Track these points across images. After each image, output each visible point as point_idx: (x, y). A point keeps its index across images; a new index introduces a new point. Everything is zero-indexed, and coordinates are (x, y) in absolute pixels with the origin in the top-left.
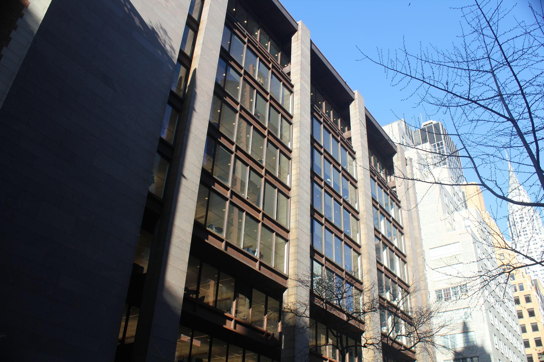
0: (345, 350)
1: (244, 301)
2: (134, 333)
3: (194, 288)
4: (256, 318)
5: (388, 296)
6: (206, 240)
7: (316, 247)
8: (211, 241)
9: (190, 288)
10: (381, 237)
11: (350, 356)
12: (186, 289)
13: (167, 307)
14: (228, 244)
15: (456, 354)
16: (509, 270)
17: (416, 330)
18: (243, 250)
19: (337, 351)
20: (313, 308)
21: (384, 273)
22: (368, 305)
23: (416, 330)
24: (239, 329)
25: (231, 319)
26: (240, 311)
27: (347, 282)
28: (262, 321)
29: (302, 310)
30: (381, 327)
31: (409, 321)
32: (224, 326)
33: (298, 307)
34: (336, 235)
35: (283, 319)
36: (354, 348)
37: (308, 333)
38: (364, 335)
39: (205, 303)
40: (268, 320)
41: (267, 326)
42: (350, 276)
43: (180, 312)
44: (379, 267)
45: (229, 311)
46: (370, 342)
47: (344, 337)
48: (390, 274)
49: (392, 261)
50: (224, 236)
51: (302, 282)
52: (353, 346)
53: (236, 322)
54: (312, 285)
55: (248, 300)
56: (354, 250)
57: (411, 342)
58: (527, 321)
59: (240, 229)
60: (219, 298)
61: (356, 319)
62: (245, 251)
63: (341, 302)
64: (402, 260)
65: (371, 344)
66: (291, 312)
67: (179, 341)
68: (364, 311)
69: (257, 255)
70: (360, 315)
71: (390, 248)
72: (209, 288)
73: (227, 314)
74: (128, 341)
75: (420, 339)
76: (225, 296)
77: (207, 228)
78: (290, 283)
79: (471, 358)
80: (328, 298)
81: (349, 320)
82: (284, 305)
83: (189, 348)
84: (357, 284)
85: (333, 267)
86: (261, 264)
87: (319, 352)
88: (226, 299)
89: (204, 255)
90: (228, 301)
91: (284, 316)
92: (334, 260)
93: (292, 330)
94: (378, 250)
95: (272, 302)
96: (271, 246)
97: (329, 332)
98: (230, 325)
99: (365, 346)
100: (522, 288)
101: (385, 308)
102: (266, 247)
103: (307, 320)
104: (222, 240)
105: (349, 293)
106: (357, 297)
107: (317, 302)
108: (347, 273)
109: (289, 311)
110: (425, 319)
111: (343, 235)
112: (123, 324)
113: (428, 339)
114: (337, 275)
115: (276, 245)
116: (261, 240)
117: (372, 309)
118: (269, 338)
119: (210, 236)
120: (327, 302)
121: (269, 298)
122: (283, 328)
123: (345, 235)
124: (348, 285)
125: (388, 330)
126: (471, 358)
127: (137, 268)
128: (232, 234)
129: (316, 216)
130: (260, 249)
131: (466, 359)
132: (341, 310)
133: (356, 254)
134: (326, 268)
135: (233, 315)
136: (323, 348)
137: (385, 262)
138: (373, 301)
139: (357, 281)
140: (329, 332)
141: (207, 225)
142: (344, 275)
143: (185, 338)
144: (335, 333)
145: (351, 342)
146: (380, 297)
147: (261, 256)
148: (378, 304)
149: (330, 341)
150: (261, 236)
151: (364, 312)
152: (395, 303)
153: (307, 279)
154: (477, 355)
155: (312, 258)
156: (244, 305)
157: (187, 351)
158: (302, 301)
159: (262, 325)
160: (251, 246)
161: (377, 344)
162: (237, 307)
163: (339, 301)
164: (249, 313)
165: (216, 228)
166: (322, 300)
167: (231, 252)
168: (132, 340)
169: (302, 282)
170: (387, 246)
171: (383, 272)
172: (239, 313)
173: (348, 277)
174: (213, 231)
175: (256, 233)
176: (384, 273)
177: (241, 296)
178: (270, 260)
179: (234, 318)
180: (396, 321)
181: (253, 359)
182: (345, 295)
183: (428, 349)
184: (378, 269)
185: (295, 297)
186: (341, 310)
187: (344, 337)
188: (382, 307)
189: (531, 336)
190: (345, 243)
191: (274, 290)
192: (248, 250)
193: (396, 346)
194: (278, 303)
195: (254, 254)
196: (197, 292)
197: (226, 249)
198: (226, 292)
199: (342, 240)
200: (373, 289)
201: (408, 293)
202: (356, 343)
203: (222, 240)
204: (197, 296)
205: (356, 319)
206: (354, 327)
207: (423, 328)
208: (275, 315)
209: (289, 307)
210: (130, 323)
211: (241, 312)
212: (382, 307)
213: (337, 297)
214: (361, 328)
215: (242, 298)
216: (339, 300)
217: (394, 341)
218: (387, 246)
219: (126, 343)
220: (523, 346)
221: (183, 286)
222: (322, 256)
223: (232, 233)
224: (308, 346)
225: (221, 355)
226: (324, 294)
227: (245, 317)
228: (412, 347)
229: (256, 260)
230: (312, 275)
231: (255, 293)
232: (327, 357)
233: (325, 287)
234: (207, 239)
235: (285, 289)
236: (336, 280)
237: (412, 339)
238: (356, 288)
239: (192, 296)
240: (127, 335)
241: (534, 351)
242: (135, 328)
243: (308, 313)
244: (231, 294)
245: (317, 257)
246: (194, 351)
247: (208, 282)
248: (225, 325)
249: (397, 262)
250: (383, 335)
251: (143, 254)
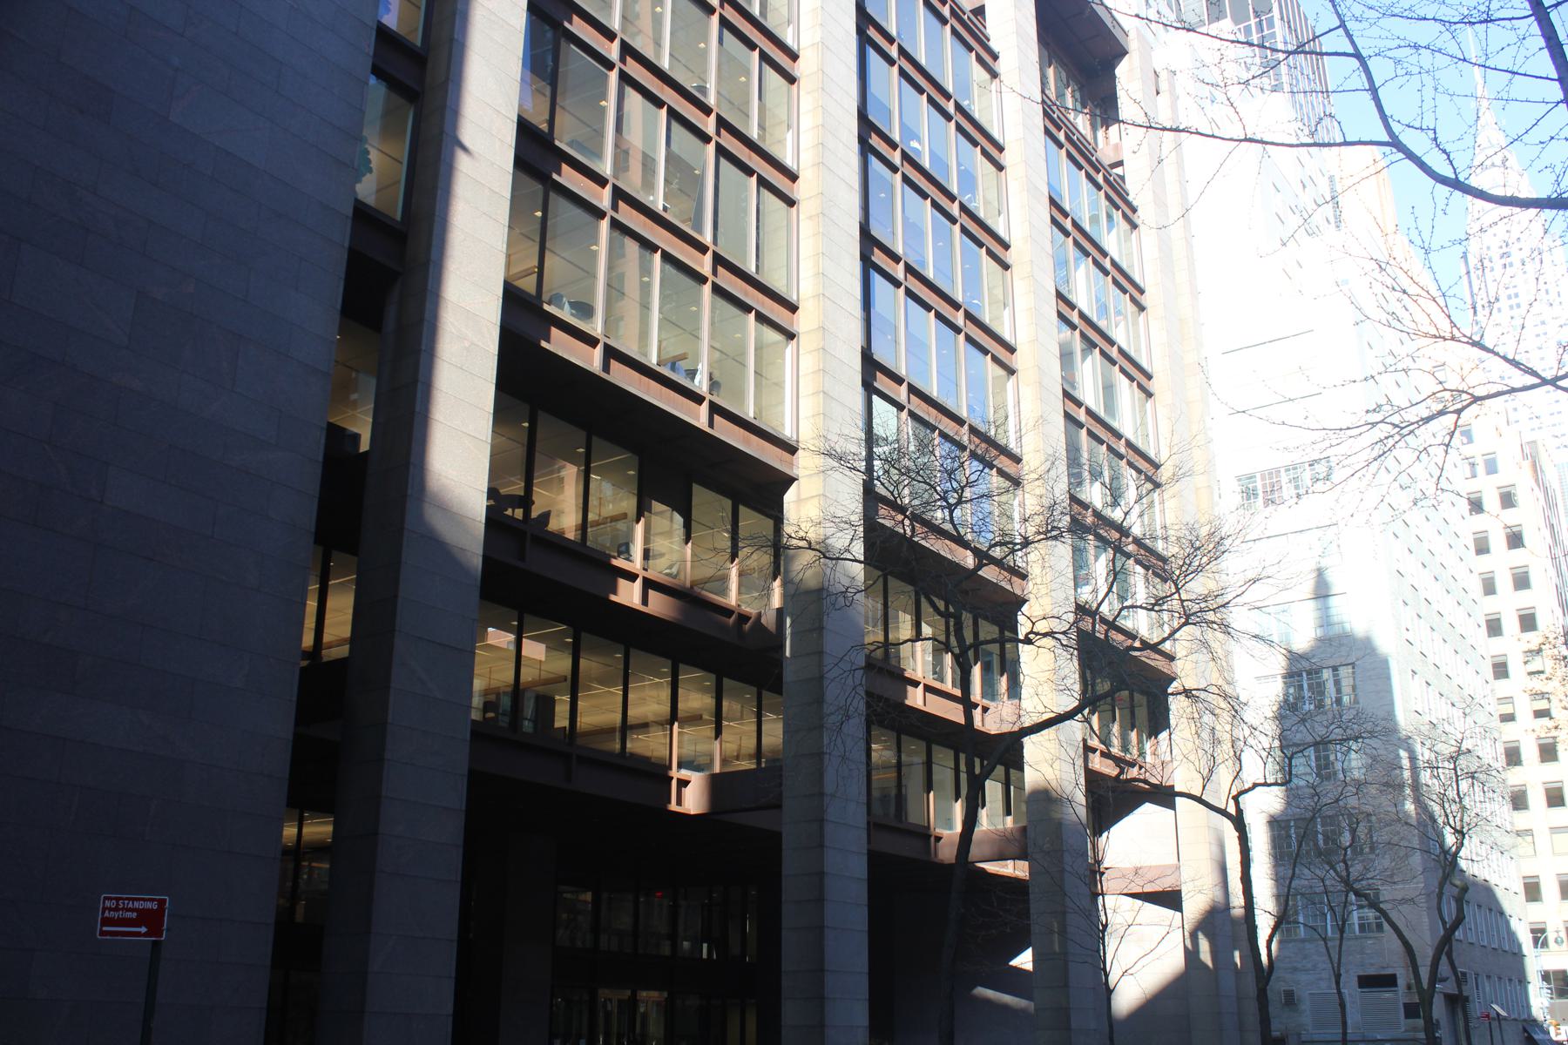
8: (559, 344)
25: (632, 577)
73: (619, 563)
135: (636, 564)
167: (622, 377)
197: (606, 368)
218: (1095, 346)
235: (789, 481)
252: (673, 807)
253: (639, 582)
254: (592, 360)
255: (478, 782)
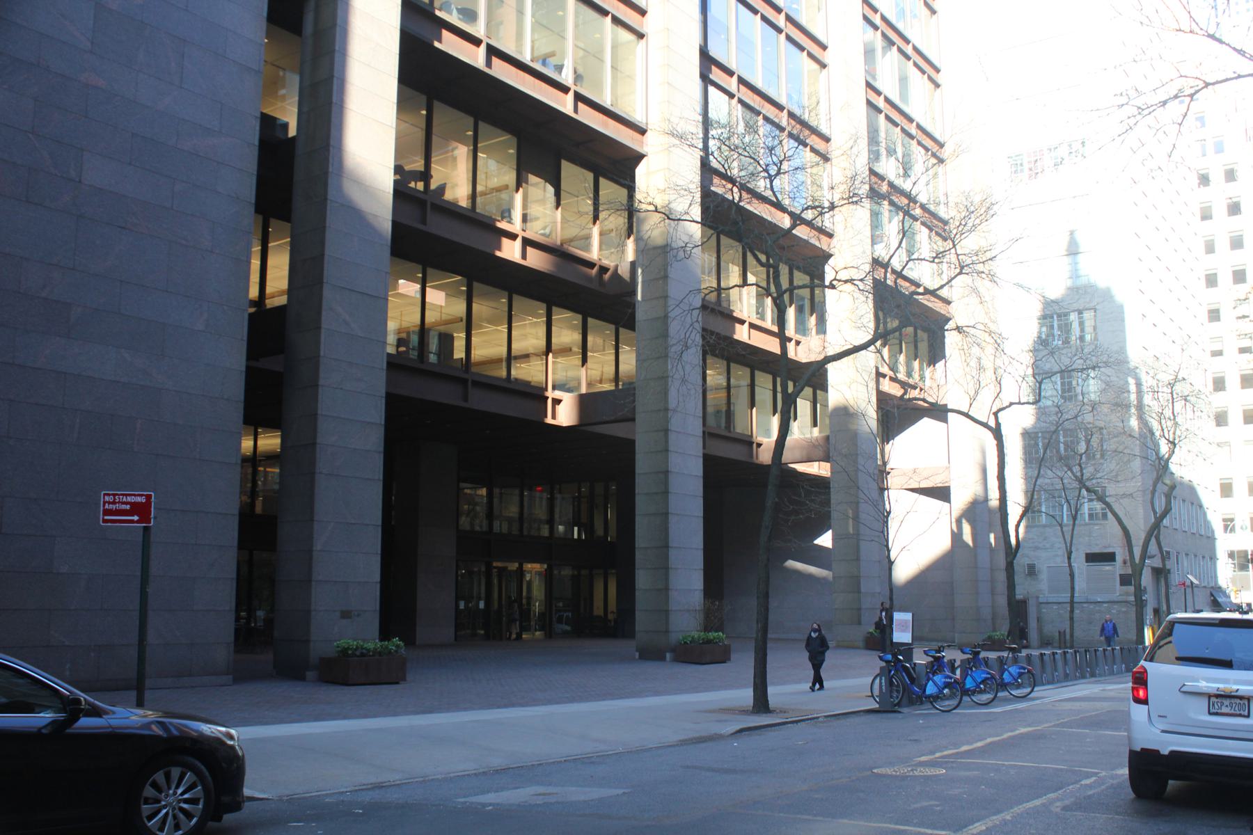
0: (786, 297)
1: (539, 189)
2: (284, 285)
3: (418, 165)
4: (572, 232)
5: (889, 168)
6: (436, 44)
7: (714, 52)
8: (449, 44)
9: (407, 168)
10: (877, 20)
11: (800, 310)
12: (398, 169)
13: (356, 215)
14: (492, 51)
15: (1048, 304)
16: (1192, 91)
17: (954, 246)
18: (531, 64)
19: (769, 301)
20: (708, 196)
21: (884, 109)
22: (843, 187)
23: (954, 246)
24: (535, 260)
25: (513, 237)
26: (534, 218)
27: (791, 135)
28: (588, 238)
29: (680, 206)
30: (872, 245)
31: (937, 225)
32: (498, 254)
33: (672, 197)
34: (764, 19)
35: (638, 231)
36: (806, 293)
37: (699, 262)
38: (831, 261)
39: (448, 202)
40: (601, 234)
41: (601, 249)
42: (804, 124)
43: (386, 225)
44: (870, 14)
45: (506, 214)
46: (843, 275)
47: (784, 270)
48: (898, 115)
49: (903, 80)
50: (479, 30)
51: (681, 137)
52: (804, 287)
53: (527, 242)
54: (706, 147)
55: (550, 190)
56: (810, 55)
57: (940, 275)
58: (1222, 226)
59: (520, 12)
60: (479, 188)
61: (809, 224)
62: (537, 66)
63: (776, 182)
64: (930, 78)
65: (846, 282)
66: (656, 211)
67: (393, 296)
68: (832, 203)
69: (566, 77)
70: (821, 214)
71: (900, 50)
72: (455, 166)
73: (502, 225)
74: (271, 303)
75: (962, 268)
76: (495, 182)
77: (438, 13)
78: (651, 145)
79: (1080, 312)
80: (743, 173)
81: (794, 226)
82: (639, 196)
83: (419, 309)
84: (813, 141)
85: (758, 98)
86: (579, 98)
87: (724, 304)
88: (499, 190)
89: (436, 82)
90: (504, 195)
91: (641, 222)
92: (759, 84)
93: (660, 257)
94: (869, 53)
95: (609, 189)
96: (602, 51)
97: (750, 258)
98: (511, 251)
99: (832, 287)
100: (1219, 149)
101: (881, 193)
102: (592, 54)
103: (696, 230)
104: (476, 42)
105: (796, 162)
106: (815, 170)
107: (718, 187)
108: (791, 115)
109: (652, 208)
110: (978, 221)
111: (782, 17)
112: (256, 263)
113: (980, 267)
114: (766, 119)
115: (615, 47)
116: (576, 38)
117: (852, 199)
118: (607, 276)
119: (445, 33)
120: (743, 188)
121: (602, 181)
122: (638, 251)
123: (789, 19)
124: (793, 143)
125: (888, 246)
126: (1080, 312)
127: (269, 124)
128: (502, 27)
129: (716, 75)
130: (575, 62)
131: (1066, 315)
132: (778, 206)
133: (816, 66)
134: (740, 101)
135: (516, 226)
136: (734, 293)
137: (888, 86)
138: (853, 178)
139: (815, 131)
140: (750, 258)
141: (436, 4)
142: (784, 120)
143: (408, 288)
144: (763, 258)
145: (801, 278)
146: (872, 172)
147: (578, 77)
148: (867, 187)
149: (751, 279)
150: (576, 26)
151: (832, 207)
152: (906, 185)
153: (694, 130)
154: (1092, 305)
155: (705, 78)
156: (542, 201)
157: (416, 318)
158: (680, 183)
159: (587, 248)
160: (552, 54)
161: (861, 280)
162: (525, 206)
163: (771, 182)
164: (555, 222)
165: (460, 11)
166: (731, 180)
167: (501, 71)
168: (282, 300)
169: (681, 137)
170: (893, 44)
171: (880, 111)
172: (531, 220)
173: (793, 123)
174: (453, 18)
175: (562, 20)
176: (884, 109)
177: (533, 179)
178: (599, 86)
179: (521, 234)
180: (907, 225)
181: (573, 328)
182: (785, 166)
183: (981, 290)
184: (869, 103)
185: (667, 180)
186: (778, 206)
187: (784, 270)
188: (874, 194)
189: (1224, 262)
190: (789, 38)
191: (615, 164)
192: (544, 63)
193: (905, 287)
194: (625, 192)
195: (560, 72)
196: (425, 176)
197: (489, 64)
198: (497, 171)
199: (779, 31)
200: (855, 150)
201: (941, 161)
202: (812, 279)
203: (476, 42)
204: (427, 185)
205: (809, 224)
206: (807, 242)
207: (968, 244)
208: (619, 221)
209: (649, 200)
210: (271, 262)
211: (537, 219)
212: (874, 194)
213: (766, 171)
214: (825, 247)
215: (535, 185)
216: (771, 179)
217: (899, 275)
219: (268, 306)
220: (1202, 248)
221: (390, 163)
222: (730, 73)
223: (501, 23)
224: (699, 290)
225: (493, 321)
226: (735, 164)
227: (547, 231)
228: (942, 287)
229: (565, 90)
230: (707, 123)
231: (569, 170)
232: (743, 316)
233: (737, 147)
234: (440, 41)
235: (639, 157)
236: (764, 128)
237: (945, 266)
238: (813, 150)
239: (415, 195)
240: (269, 290)
241: (1237, 399)
242: (286, 272)
243: (696, 213)
244: (510, 177)
245: (716, 75)
246: (431, 317)
247: (453, 150)
248: (500, 250)
249: (918, 82)
250: (876, 262)
251: (283, 92)
252: (549, 420)
253: (746, 325)
254: (476, 57)
255: (394, 403)
